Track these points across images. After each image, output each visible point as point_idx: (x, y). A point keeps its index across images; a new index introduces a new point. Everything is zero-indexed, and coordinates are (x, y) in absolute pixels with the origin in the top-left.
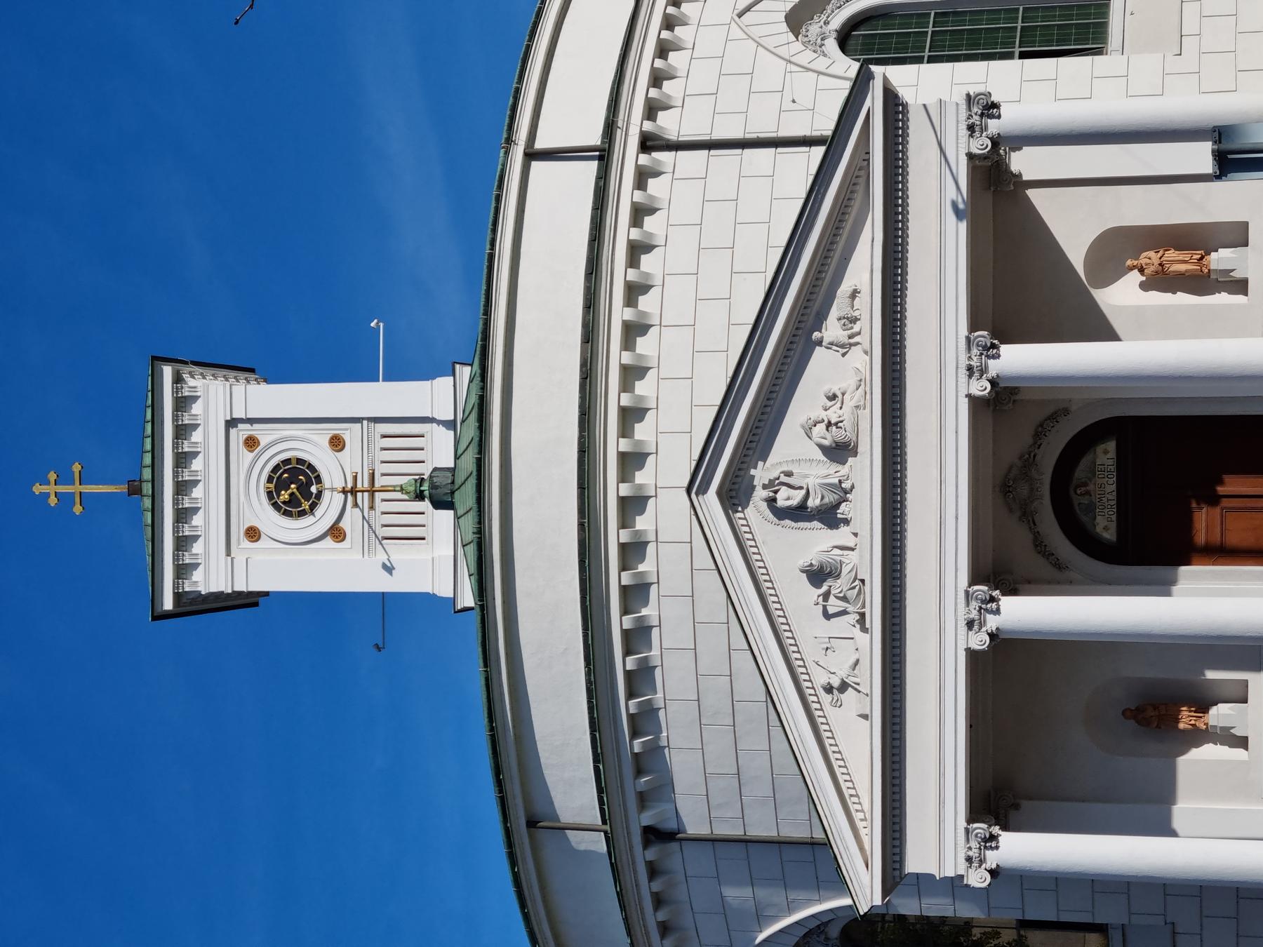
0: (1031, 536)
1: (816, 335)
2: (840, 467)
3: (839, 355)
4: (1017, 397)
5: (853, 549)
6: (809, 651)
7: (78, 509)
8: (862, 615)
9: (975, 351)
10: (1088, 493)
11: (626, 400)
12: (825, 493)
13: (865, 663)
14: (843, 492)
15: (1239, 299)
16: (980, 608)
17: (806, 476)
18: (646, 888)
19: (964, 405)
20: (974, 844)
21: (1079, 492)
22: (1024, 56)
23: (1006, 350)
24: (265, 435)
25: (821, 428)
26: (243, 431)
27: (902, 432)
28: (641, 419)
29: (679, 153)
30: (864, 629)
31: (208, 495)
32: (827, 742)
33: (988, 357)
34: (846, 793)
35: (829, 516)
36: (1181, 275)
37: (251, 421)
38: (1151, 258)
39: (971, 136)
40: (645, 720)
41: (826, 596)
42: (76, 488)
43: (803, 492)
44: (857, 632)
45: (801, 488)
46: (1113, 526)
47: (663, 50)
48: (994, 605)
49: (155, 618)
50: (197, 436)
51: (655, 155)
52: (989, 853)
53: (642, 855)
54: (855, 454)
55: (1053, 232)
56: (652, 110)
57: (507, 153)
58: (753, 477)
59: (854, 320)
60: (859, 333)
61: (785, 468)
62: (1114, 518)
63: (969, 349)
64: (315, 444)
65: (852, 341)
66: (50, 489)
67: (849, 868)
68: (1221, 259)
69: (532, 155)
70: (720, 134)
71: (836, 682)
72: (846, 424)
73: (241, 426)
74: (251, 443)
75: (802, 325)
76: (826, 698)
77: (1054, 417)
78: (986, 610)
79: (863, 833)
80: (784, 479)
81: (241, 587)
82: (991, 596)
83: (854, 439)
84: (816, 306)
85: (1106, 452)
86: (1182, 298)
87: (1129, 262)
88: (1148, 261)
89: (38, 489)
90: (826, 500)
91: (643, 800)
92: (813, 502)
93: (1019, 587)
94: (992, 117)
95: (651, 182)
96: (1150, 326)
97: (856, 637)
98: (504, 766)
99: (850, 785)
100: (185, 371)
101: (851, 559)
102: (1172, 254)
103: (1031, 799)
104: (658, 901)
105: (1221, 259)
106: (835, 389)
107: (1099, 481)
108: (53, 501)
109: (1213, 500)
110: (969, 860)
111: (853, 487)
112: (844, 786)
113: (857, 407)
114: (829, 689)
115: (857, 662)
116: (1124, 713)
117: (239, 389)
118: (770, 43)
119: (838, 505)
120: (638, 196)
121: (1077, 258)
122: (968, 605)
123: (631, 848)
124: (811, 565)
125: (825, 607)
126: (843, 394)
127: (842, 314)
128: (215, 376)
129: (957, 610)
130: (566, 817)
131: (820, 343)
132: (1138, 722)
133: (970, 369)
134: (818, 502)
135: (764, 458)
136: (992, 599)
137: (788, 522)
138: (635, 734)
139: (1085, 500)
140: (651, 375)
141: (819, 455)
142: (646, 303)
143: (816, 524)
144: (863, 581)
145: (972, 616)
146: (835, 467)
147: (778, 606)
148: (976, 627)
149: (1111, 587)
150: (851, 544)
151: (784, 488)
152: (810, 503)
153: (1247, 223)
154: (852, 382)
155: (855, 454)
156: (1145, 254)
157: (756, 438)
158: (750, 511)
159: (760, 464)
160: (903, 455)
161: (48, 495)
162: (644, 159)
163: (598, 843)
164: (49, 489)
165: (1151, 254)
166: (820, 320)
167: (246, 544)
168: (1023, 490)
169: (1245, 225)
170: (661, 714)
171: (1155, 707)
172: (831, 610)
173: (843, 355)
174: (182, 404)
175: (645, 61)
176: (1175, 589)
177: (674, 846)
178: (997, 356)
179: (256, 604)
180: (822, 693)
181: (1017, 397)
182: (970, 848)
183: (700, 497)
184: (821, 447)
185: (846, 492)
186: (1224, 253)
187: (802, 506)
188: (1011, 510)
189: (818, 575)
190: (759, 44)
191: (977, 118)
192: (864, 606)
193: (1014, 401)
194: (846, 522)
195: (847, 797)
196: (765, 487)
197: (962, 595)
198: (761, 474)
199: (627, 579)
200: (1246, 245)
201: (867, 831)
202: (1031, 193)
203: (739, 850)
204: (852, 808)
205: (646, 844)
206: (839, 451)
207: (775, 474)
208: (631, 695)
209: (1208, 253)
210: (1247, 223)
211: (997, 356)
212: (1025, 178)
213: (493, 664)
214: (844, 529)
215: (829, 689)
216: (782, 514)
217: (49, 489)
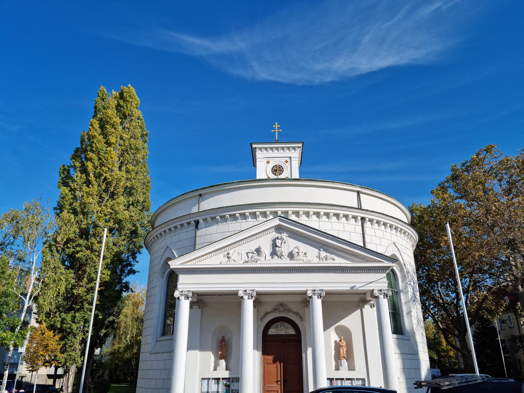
0: (269, 311)
1: (322, 249)
2: (287, 256)
3: (317, 255)
4: (305, 307)
5: (265, 260)
6: (238, 249)
7: (272, 131)
8: (248, 262)
9: (319, 292)
10: (281, 327)
11: (301, 213)
12: (280, 252)
13: (235, 263)
14: (280, 257)
15: (334, 368)
16: (250, 294)
17: (284, 247)
18: (184, 222)
19: (305, 289)
20: (186, 293)
21: (281, 324)
22: (389, 312)
23: (320, 301)
24: (288, 164)
25: (297, 251)
26: (288, 159)
27: (297, 272)
28: (296, 216)
29: (361, 227)
30: (244, 263)
31: (276, 153)
32: (214, 253)
33: (318, 295)
34: (200, 259)
35: (274, 253)
36: (340, 352)
37: (291, 162)
38: (344, 343)
39: (378, 290)
40: (224, 219)
41: (253, 253)
42: (277, 131)
43: (280, 246)
44: (243, 261)
45: (281, 246)
46: (272, 333)
47: (385, 224)
48: (250, 298)
49: (251, 144)
50: (287, 151)
51: (360, 221)
52: (184, 297)
53: (192, 220)
54: (290, 260)
55: (350, 316)
56: (371, 221)
57: (359, 187)
58: (284, 233)
59: (326, 259)
60: (323, 261)
61: (286, 242)
62: (275, 334)
63: (320, 290)
64: (286, 174)
65: (321, 259)
66: (276, 126)
67: (180, 259)
68: (345, 363)
69: (358, 193)
70: (366, 236)
71: (230, 256)
72: (298, 257)
73: (290, 160)
74: (287, 162)
75: (324, 246)
76: (226, 253)
77: (300, 317)
78: (249, 295)
79: (190, 263)
80: (284, 241)
81: (257, 160)
82: (253, 297)
83: (295, 259)
84: (330, 249)
85: (292, 331)
86: (333, 352)
87: (342, 337)
88: (343, 343)
89: (276, 123)
90: (278, 252)
91: (205, 220)
92: (277, 249)
93: (256, 309)
94: (384, 296)
95: (354, 220)
96: (327, 340)
97: (242, 261)
98: (213, 188)
99: (203, 260)
100: (301, 149)
101: (262, 259)
102: (345, 349)
103: (201, 312)
104: (182, 225)
105: (345, 363)
106: (308, 255)
107: (284, 330)
108: (274, 126)
109: (274, 361)
110: (182, 292)
111: (282, 259)
112: (202, 258)
113: (303, 260)
114: (228, 254)
115: (235, 261)
116: (223, 336)
117: (297, 159)
118: (388, 250)
119: (277, 255)
120: (350, 216)
121: (342, 323)
122: (251, 290)
123: (194, 217)
124: (261, 249)
125: (250, 253)
126: (306, 257)
127: (328, 256)
128: (299, 156)
129: (249, 288)
130: (202, 204)
131: (320, 250)
132: (221, 340)
133: (315, 290)
134: (278, 250)
135: (289, 237)
136: (252, 297)
137: (272, 243)
138: (221, 217)
139: (279, 326)
140: (307, 219)
141: (290, 251)
142: (325, 218)
143: (272, 250)
144: (257, 262)
145: (247, 291)
146: (287, 255)
147: (250, 240)
148: (244, 293)
149: (256, 333)
150: (266, 259)
151: (281, 241)
152: (277, 248)
153: (355, 370)
154: (309, 259)
155: (290, 260)
156: (344, 341)
157: (294, 234)
158: (274, 233)
159: (287, 235)
160: (291, 273)
161: (275, 125)
162: (359, 218)
163: (195, 210)
164: (276, 125)
165: (345, 344)
166: (326, 251)
167: (266, 161)
168: (281, 309)
169: (354, 370)
170: (226, 223)
171: (225, 345)
172: (249, 254)
173: (317, 257)
174: (294, 148)
175: (383, 220)
176: (256, 351)
177: (194, 228)
178: (318, 298)
179: (254, 166)
180: (227, 252)
181: (305, 307)
182: (185, 292)
183: (278, 219)
184: (292, 251)
185: (280, 257)
186: (346, 364)
187: (276, 246)
188: (276, 306)
189: (258, 251)
190: (388, 247)
191: (384, 292)
192: (250, 262)
193: (304, 306)
194: (272, 258)
195: (200, 259)
196: (281, 237)
197: (253, 289)
198: (284, 235)
199: (258, 213)
200: (349, 370)
201: (190, 264)
202: (359, 311)
203: (194, 244)
204: (197, 260)
205: (195, 221)
206: (291, 256)
207: (284, 239)
208: (230, 215)
209: (346, 359)
210: (355, 370)
211: (318, 298)
212: (363, 309)
213: (238, 183)
214: (270, 257)
215: (228, 254)
216: (274, 241)
217: (276, 125)
